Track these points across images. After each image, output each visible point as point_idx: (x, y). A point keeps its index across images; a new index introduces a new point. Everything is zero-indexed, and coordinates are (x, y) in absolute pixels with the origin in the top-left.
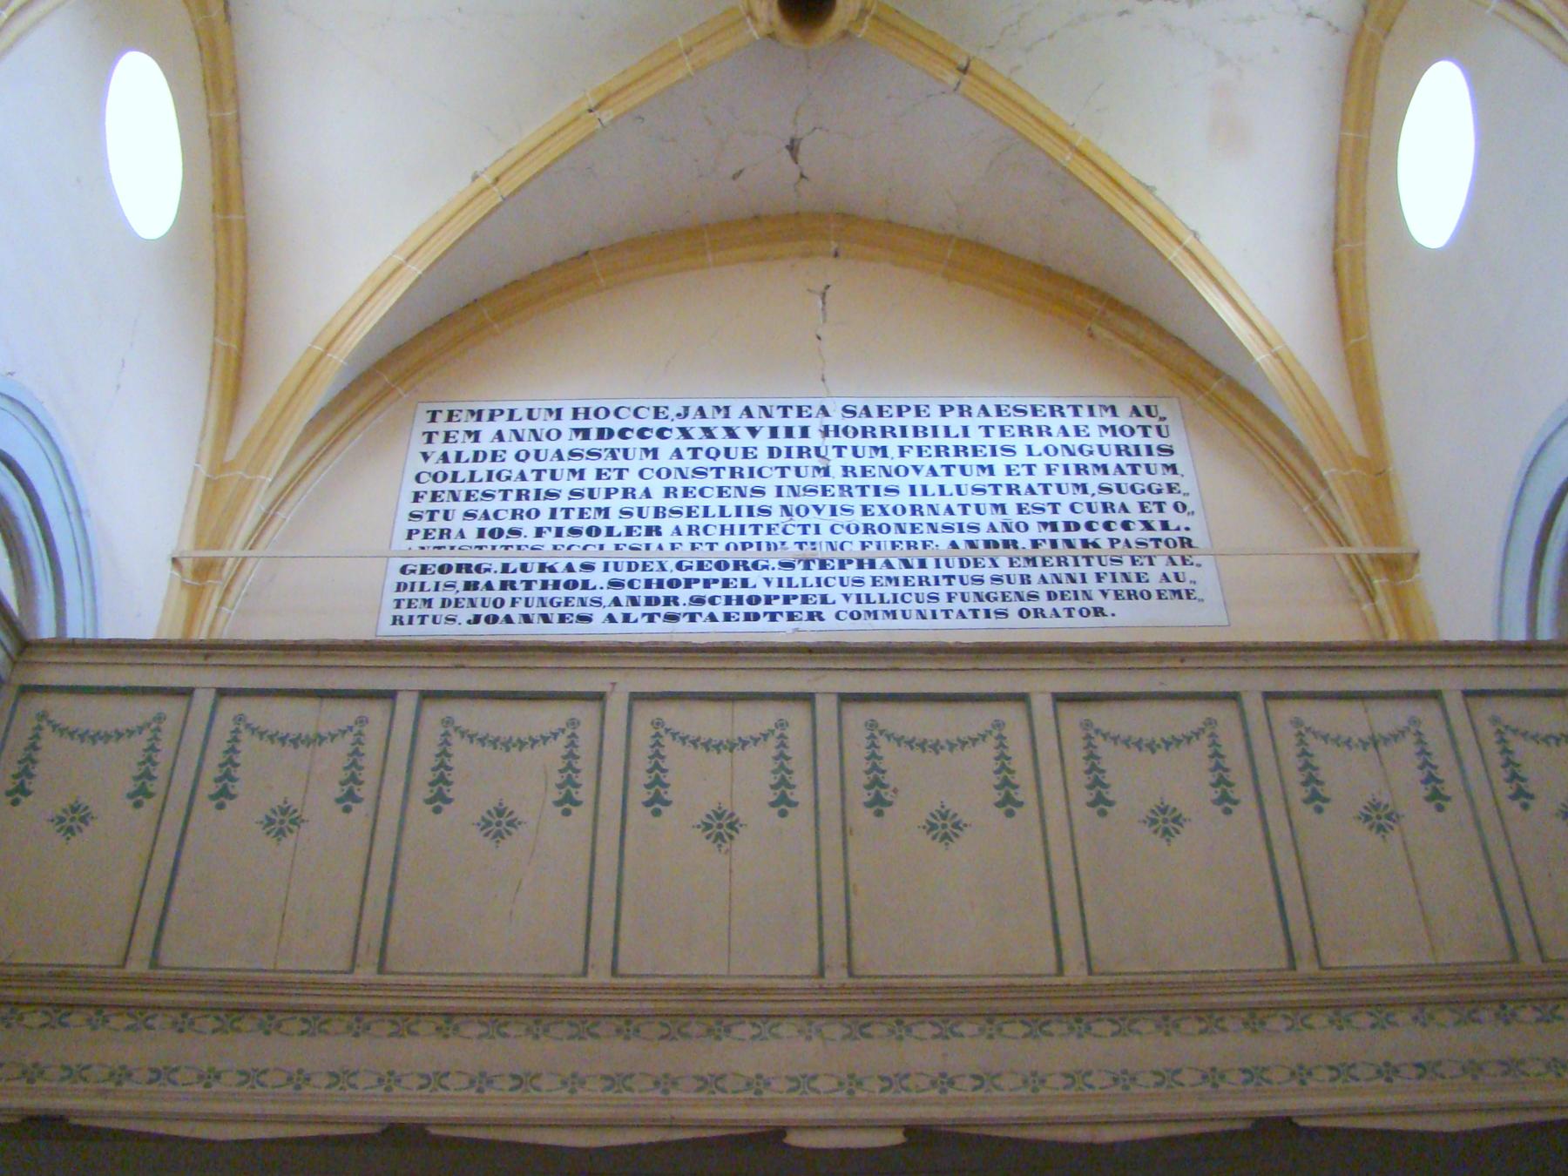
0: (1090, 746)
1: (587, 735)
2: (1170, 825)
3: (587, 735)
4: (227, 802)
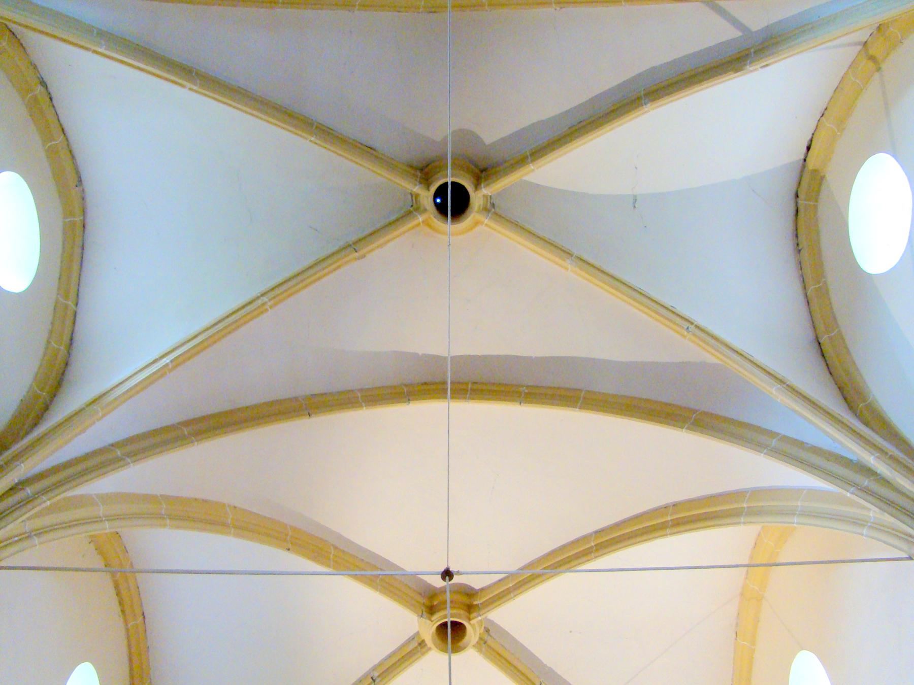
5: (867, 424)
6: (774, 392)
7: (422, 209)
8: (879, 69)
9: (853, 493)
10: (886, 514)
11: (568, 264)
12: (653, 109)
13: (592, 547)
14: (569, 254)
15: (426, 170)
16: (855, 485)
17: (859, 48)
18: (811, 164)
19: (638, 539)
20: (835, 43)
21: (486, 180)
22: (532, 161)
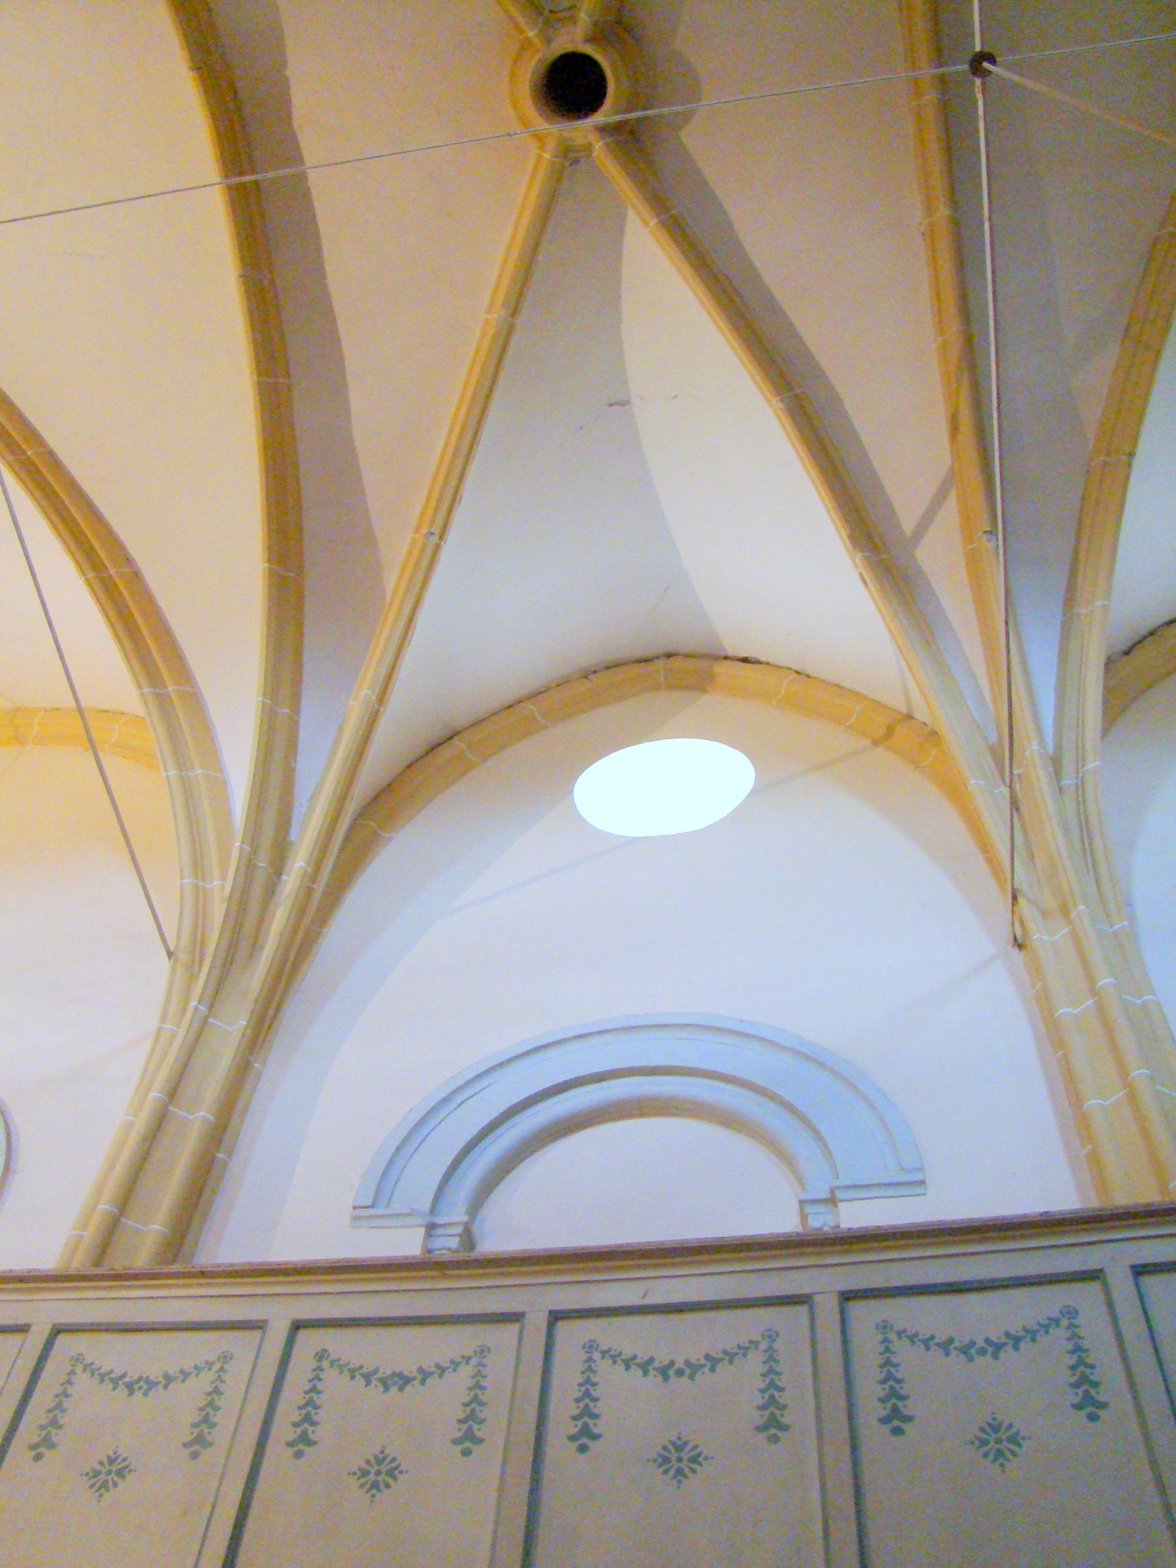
0: (589, 1367)
1: (500, 1368)
2: (685, 1456)
3: (500, 1368)
4: (307, 1449)
5: (348, 838)
6: (363, 693)
7: (551, 32)
8: (875, 743)
9: (241, 850)
10: (225, 906)
11: (499, 313)
12: (775, 411)
13: (23, 452)
14: (515, 312)
15: (621, 32)
16: (255, 851)
17: (904, 711)
18: (722, 668)
19: (61, 526)
20: (907, 674)
21: (618, 143)
22: (662, 223)
